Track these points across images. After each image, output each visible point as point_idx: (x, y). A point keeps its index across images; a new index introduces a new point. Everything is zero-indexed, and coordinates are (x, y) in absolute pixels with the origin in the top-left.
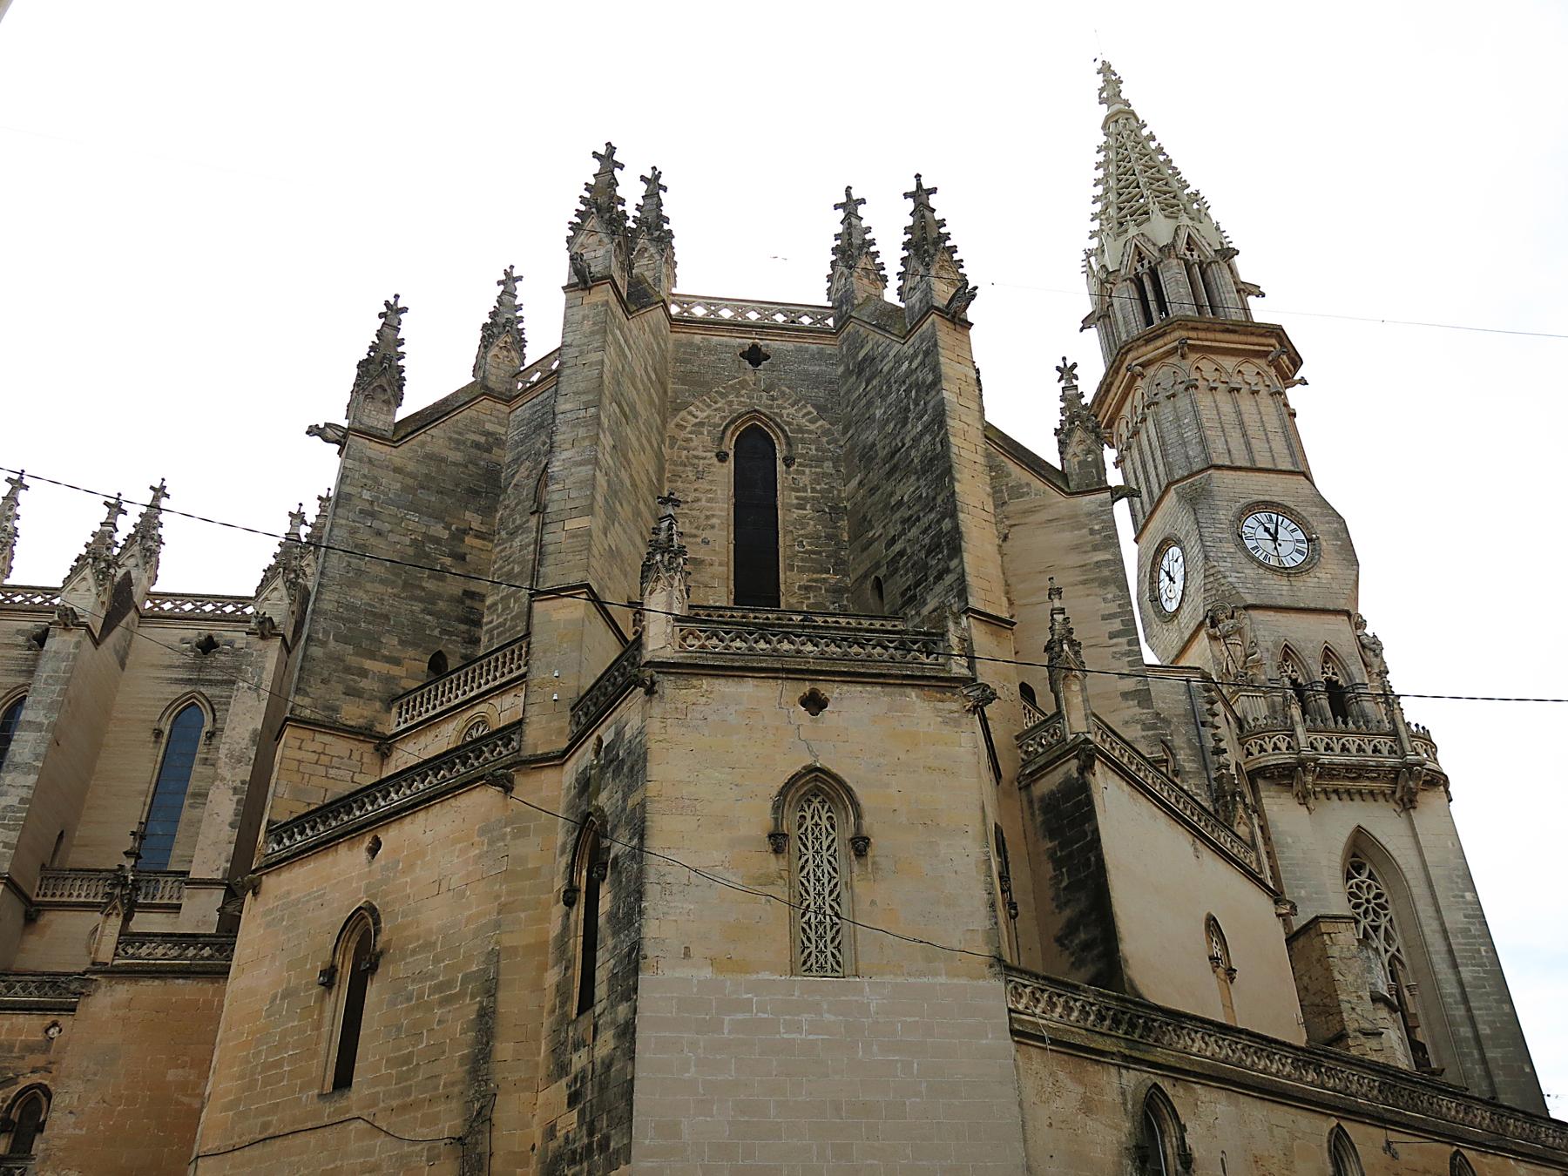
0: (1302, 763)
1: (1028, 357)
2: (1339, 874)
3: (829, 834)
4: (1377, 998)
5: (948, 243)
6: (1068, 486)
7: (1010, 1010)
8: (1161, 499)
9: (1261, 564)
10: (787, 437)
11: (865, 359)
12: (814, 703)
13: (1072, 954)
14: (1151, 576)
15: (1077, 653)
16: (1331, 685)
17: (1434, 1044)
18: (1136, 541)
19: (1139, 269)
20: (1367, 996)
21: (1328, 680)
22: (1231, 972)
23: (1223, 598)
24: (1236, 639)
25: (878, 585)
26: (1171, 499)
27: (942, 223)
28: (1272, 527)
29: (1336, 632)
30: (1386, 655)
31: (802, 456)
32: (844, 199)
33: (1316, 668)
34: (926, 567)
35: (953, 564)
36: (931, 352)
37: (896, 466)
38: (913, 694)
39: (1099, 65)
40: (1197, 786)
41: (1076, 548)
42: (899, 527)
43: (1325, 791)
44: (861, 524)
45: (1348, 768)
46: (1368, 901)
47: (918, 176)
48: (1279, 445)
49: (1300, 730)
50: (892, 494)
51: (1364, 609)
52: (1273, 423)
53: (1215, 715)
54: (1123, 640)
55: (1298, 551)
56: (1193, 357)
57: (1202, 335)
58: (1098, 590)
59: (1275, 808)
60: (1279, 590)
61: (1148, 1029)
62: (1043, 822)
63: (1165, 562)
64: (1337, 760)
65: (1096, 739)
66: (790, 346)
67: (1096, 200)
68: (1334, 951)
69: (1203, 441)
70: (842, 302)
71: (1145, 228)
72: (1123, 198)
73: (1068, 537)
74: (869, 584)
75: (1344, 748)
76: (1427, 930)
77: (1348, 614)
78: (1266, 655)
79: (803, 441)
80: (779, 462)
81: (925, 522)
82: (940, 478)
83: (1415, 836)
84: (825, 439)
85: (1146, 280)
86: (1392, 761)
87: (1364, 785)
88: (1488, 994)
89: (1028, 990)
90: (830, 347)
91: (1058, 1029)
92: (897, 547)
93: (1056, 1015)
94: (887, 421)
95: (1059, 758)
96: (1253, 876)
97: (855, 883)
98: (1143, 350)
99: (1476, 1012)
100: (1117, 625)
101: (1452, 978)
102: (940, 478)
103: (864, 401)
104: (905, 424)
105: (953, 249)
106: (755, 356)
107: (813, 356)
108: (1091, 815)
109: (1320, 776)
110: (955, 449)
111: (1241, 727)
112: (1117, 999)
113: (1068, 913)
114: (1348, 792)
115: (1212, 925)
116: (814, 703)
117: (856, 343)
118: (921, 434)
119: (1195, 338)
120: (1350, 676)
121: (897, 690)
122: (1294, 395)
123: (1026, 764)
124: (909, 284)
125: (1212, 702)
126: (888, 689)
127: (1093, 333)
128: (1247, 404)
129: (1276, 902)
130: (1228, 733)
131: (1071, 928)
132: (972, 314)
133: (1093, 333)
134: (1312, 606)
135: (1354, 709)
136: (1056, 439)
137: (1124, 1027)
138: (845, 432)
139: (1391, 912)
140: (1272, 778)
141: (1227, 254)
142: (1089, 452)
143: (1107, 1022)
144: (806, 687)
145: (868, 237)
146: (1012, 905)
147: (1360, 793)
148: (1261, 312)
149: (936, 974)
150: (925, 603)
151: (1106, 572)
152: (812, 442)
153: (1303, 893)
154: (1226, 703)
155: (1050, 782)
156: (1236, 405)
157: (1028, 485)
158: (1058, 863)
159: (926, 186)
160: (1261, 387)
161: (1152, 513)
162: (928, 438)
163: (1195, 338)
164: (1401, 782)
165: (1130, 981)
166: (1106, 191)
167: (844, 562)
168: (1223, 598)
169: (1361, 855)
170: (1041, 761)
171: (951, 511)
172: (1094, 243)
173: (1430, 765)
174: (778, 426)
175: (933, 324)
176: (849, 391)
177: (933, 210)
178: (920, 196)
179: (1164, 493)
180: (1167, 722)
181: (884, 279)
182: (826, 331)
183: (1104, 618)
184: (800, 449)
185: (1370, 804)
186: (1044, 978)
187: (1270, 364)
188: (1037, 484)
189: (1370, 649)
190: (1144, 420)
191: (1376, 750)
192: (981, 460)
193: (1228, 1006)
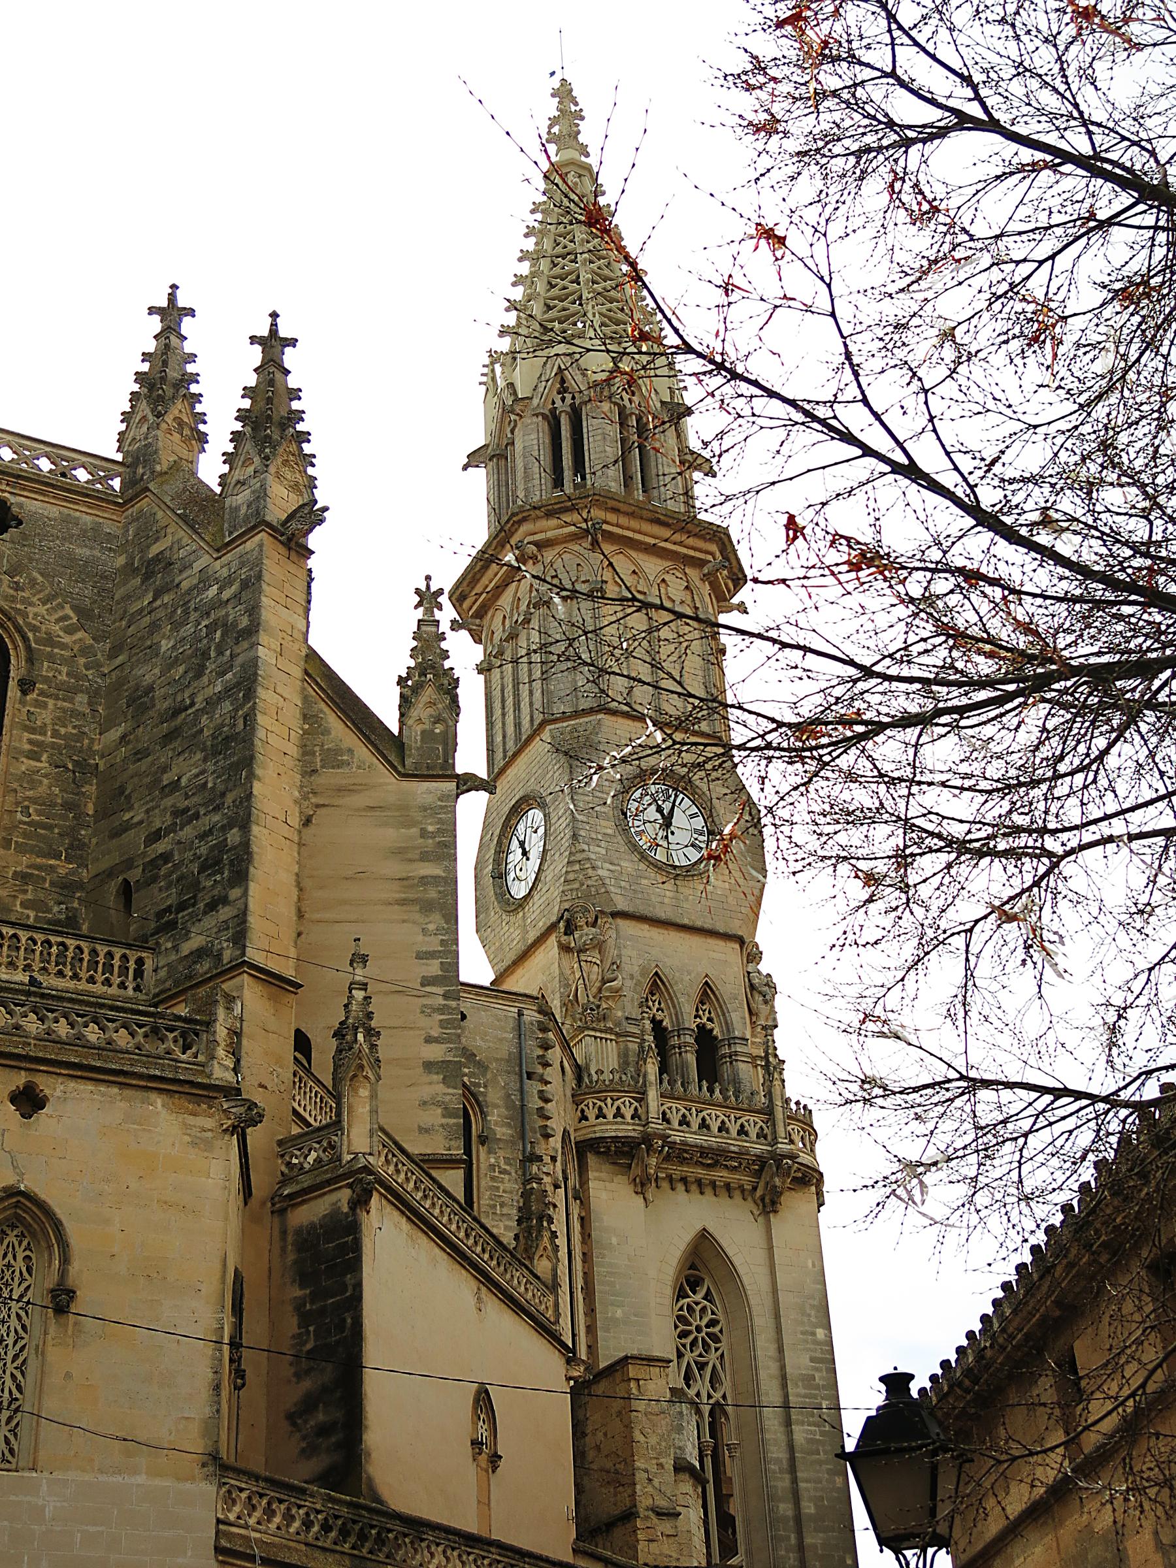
0: (647, 1139)
1: (383, 563)
2: (669, 1292)
3: (23, 1279)
4: (681, 1467)
7: (219, 1521)
8: (530, 739)
9: (643, 857)
10: (29, 648)
11: (158, 558)
12: (29, 1102)
13: (304, 1438)
14: (499, 843)
15: (373, 1047)
16: (704, 1036)
17: (747, 1522)
19: (559, 403)
20: (669, 1463)
21: (701, 1027)
22: (495, 1458)
23: (588, 896)
25: (126, 891)
26: (540, 747)
27: (295, 394)
28: (667, 807)
29: (717, 961)
30: (779, 1002)
31: (46, 680)
32: (164, 303)
33: (688, 1009)
34: (196, 886)
35: (234, 893)
36: (251, 584)
37: (177, 730)
38: (158, 1101)
39: (555, 83)
40: (507, 1161)
41: (399, 853)
42: (169, 820)
43: (670, 1178)
44: (116, 798)
45: (704, 1151)
47: (274, 315)
49: (652, 1094)
50: (165, 769)
51: (764, 937)
53: (546, 1065)
54: (440, 990)
57: (623, 520)
58: (417, 917)
59: (604, 1196)
60: (662, 897)
61: (380, 1541)
62: (295, 1262)
63: (521, 827)
64: (691, 1138)
65: (377, 1162)
66: (54, 511)
67: (519, 280)
70: (138, 459)
72: (555, 292)
73: (391, 835)
74: (113, 886)
75: (704, 1125)
76: (763, 1374)
77: (741, 941)
78: (628, 983)
79: (51, 658)
80: (12, 684)
81: (205, 823)
82: (236, 768)
83: (770, 1249)
84: (82, 661)
86: (760, 1148)
88: (820, 1463)
89: (244, 1495)
90: (110, 522)
91: (272, 1544)
92: (161, 847)
93: (273, 1526)
94: (175, 662)
95: (329, 1182)
96: (546, 1330)
97: (49, 1348)
98: (544, 523)
99: (802, 1485)
100: (433, 968)
101: (782, 1437)
102: (236, 768)
103: (147, 620)
104: (199, 674)
105: (305, 437)
107: (84, 532)
108: (355, 1265)
109: (667, 1158)
110: (261, 733)
111: (579, 1079)
112: (350, 1505)
113: (307, 1384)
114: (699, 1183)
115: (483, 1400)
116: (29, 1102)
117: (148, 531)
118: (219, 698)
119: (614, 524)
120: (728, 1027)
121: (139, 1094)
123: (285, 1180)
124: (238, 475)
125: (546, 1047)
126: (128, 1092)
129: (568, 1361)
130: (558, 1085)
131: (308, 1405)
132: (314, 540)
133: (479, 476)
134: (699, 924)
135: (726, 1070)
136: (398, 690)
137: (352, 1539)
138: (112, 656)
139: (723, 1345)
140: (606, 1153)
142: (438, 720)
143: (333, 1534)
144: (20, 1079)
145: (190, 368)
146: (239, 1373)
147: (713, 1184)
149: (135, 1472)
150: (187, 937)
151: (432, 894)
152: (64, 661)
153: (619, 1313)
154: (566, 1046)
157: (350, 751)
158: (305, 1319)
159: (283, 333)
161: (515, 755)
162: (227, 706)
163: (614, 524)
164: (765, 1176)
165: (370, 1480)
166: (533, 274)
167: (82, 846)
168: (588, 896)
169: (702, 1266)
170: (306, 1181)
171: (243, 820)
172: (504, 345)
173: (804, 1158)
174: (19, 630)
175: (261, 545)
176: (127, 597)
177: (287, 372)
178: (273, 345)
179: (536, 732)
180: (482, 1067)
181: (203, 438)
183: (420, 956)
184: (45, 669)
185: (724, 1200)
186: (266, 1480)
187: (705, 578)
188: (363, 752)
189: (761, 991)
190: (527, 621)
191: (742, 1131)
192: (293, 750)
193: (485, 1503)
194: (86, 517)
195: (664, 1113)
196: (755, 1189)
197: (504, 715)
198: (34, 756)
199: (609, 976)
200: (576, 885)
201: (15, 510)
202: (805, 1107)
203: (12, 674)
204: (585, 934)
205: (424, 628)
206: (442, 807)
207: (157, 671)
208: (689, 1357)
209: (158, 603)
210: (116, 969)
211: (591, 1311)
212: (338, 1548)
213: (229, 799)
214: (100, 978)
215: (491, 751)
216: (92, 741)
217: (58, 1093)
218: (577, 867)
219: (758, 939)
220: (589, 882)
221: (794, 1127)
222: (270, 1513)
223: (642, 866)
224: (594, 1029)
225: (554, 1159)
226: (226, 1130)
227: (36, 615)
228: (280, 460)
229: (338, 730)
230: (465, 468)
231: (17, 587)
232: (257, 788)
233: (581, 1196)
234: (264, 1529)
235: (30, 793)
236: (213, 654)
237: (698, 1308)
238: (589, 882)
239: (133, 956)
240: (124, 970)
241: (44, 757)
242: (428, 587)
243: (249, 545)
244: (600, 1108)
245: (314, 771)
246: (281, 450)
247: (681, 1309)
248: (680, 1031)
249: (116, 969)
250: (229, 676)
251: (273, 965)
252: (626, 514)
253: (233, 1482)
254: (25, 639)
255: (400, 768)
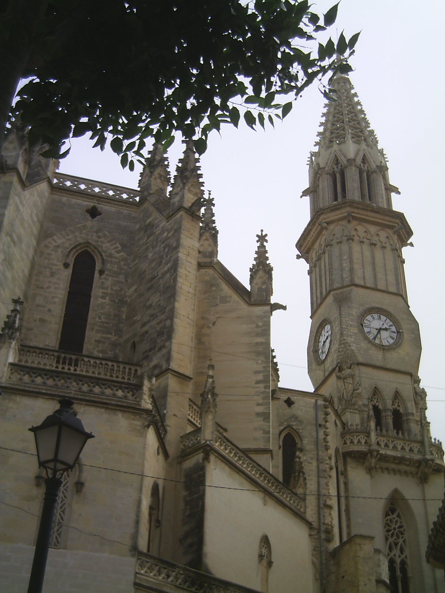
0: (371, 452)
4: (380, 582)
5: (199, 172)
6: (250, 301)
10: (103, 259)
15: (214, 400)
16: (397, 415)
18: (311, 317)
19: (336, 169)
20: (373, 579)
22: (270, 564)
24: (350, 381)
25: (134, 345)
26: (330, 299)
33: (389, 403)
35: (167, 344)
36: (178, 231)
38: (120, 415)
43: (381, 468)
45: (395, 458)
46: (395, 529)
48: (391, 278)
49: (373, 435)
50: (148, 300)
51: (421, 374)
52: (390, 265)
54: (262, 385)
55: (392, 338)
56: (354, 223)
57: (361, 212)
60: (377, 356)
68: (361, 554)
69: (351, 270)
71: (343, 146)
72: (335, 127)
74: (130, 344)
77: (411, 375)
84: (122, 263)
85: (338, 176)
86: (418, 457)
87: (403, 467)
92: (145, 328)
96: (300, 516)
98: (330, 214)
100: (260, 377)
103: (145, 247)
104: (160, 265)
105: (201, 176)
106: (93, 213)
109: (380, 460)
110: (179, 285)
112: (195, 573)
114: (387, 469)
118: (166, 272)
120: (406, 408)
122: (406, 251)
125: (327, 414)
127: (307, 199)
128: (378, 254)
133: (307, 199)
141: (383, 169)
142: (264, 283)
148: (397, 204)
150: (151, 360)
151: (260, 349)
154: (338, 416)
155: (189, 463)
156: (350, 248)
157: (230, 297)
160: (388, 245)
162: (168, 275)
171: (171, 316)
173: (438, 461)
175: (181, 216)
179: (328, 294)
180: (301, 422)
182: (134, 203)
184: (109, 266)
187: (395, 232)
188: (235, 297)
189: (420, 396)
190: (324, 253)
191: (411, 450)
194: (125, 211)
195: (378, 442)
196: (417, 473)
197: (316, 289)
198: (103, 298)
199: (355, 388)
200: (343, 353)
201: (99, 209)
202: (438, 441)
203: (96, 268)
204: (347, 372)
205: (260, 249)
206: (265, 316)
207: (147, 265)
208: (390, 540)
209: (149, 240)
210: (127, 373)
211: (348, 519)
212: (190, 589)
213: (168, 309)
214: (120, 376)
215: (312, 304)
216: (125, 291)
217: (82, 411)
218: (343, 346)
219: (419, 375)
220: (348, 352)
221: (433, 449)
222: (159, 572)
223: (370, 345)
224: (350, 409)
225: (330, 458)
226: (146, 426)
227: (106, 247)
228: (190, 185)
229: (226, 289)
230: (301, 197)
231: (99, 237)
232: (177, 305)
233: (344, 473)
234: (153, 578)
235: (101, 311)
236: (164, 257)
237: (394, 520)
238: (348, 352)
239: (133, 369)
240: (130, 373)
241: (107, 298)
242: (262, 234)
243: (178, 216)
244: (352, 440)
245: (217, 305)
246: (190, 180)
247: (387, 520)
248: (386, 410)
249: (127, 373)
250: (169, 265)
251: (181, 371)
252: (362, 209)
253: (144, 559)
254: (101, 255)
255: (249, 302)
